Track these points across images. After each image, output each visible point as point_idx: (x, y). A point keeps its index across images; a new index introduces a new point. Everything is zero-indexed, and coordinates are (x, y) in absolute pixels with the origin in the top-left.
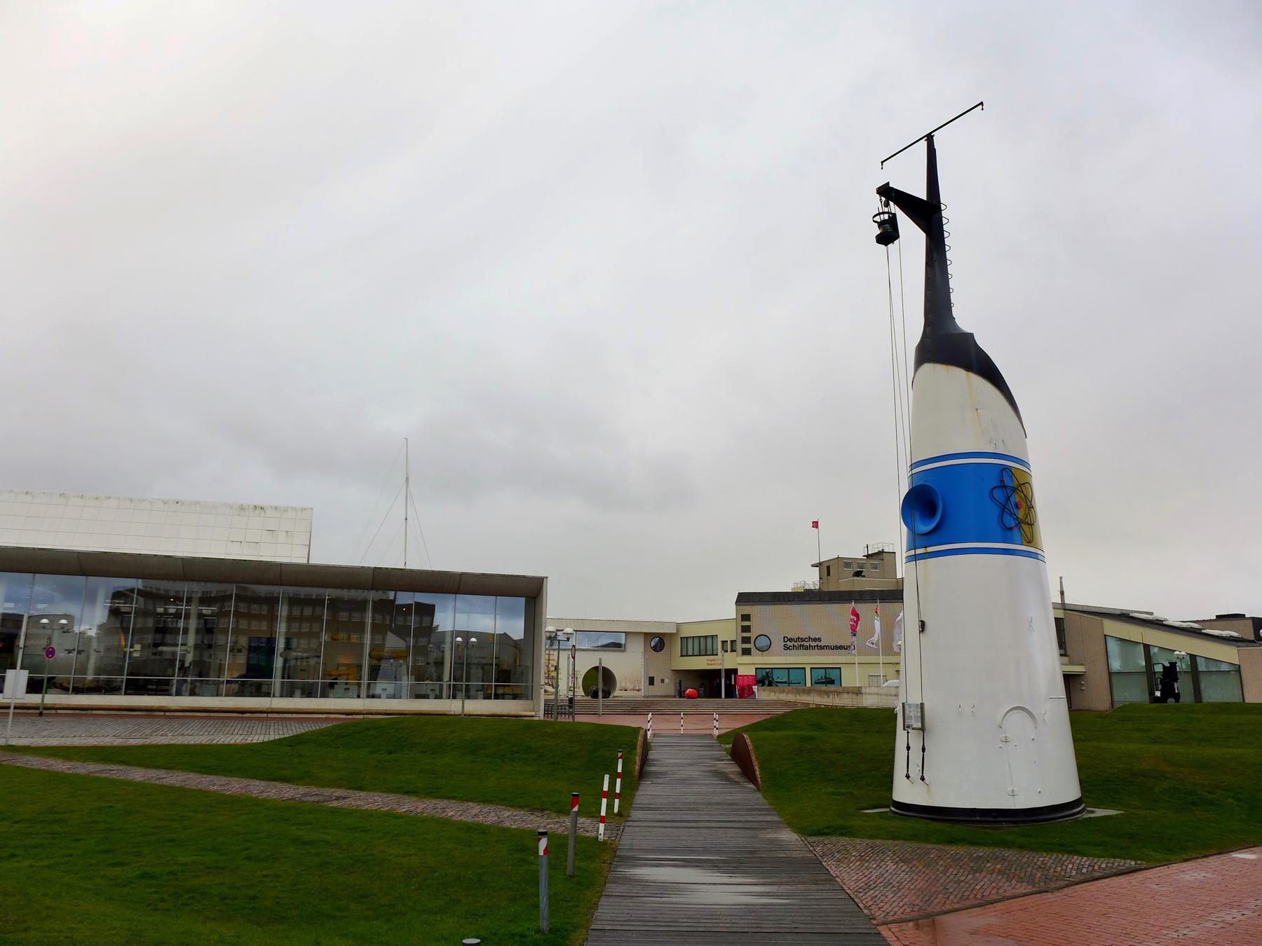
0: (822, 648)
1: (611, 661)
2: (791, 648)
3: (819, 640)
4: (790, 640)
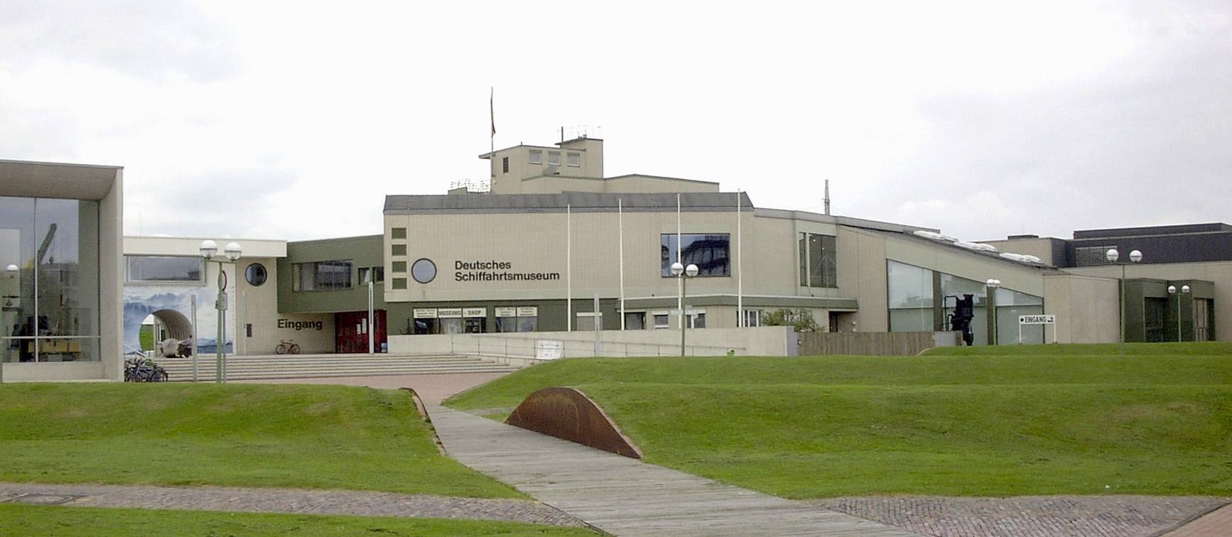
0: (512, 277)
1: (182, 297)
2: (466, 278)
3: (508, 265)
4: (464, 266)
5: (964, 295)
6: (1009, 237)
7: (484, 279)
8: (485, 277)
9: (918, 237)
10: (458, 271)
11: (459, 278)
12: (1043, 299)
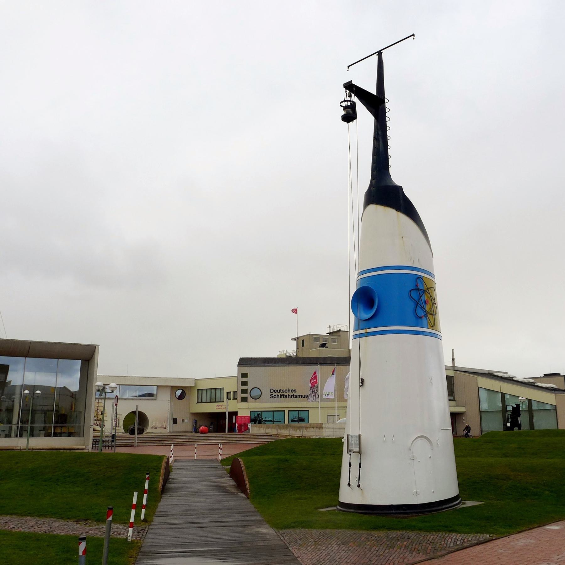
0: (297, 397)
2: (275, 397)
3: (295, 391)
4: (275, 391)
5: (516, 404)
6: (544, 375)
7: (284, 398)
8: (284, 396)
9: (495, 376)
10: (272, 393)
11: (272, 397)
12: (556, 406)
